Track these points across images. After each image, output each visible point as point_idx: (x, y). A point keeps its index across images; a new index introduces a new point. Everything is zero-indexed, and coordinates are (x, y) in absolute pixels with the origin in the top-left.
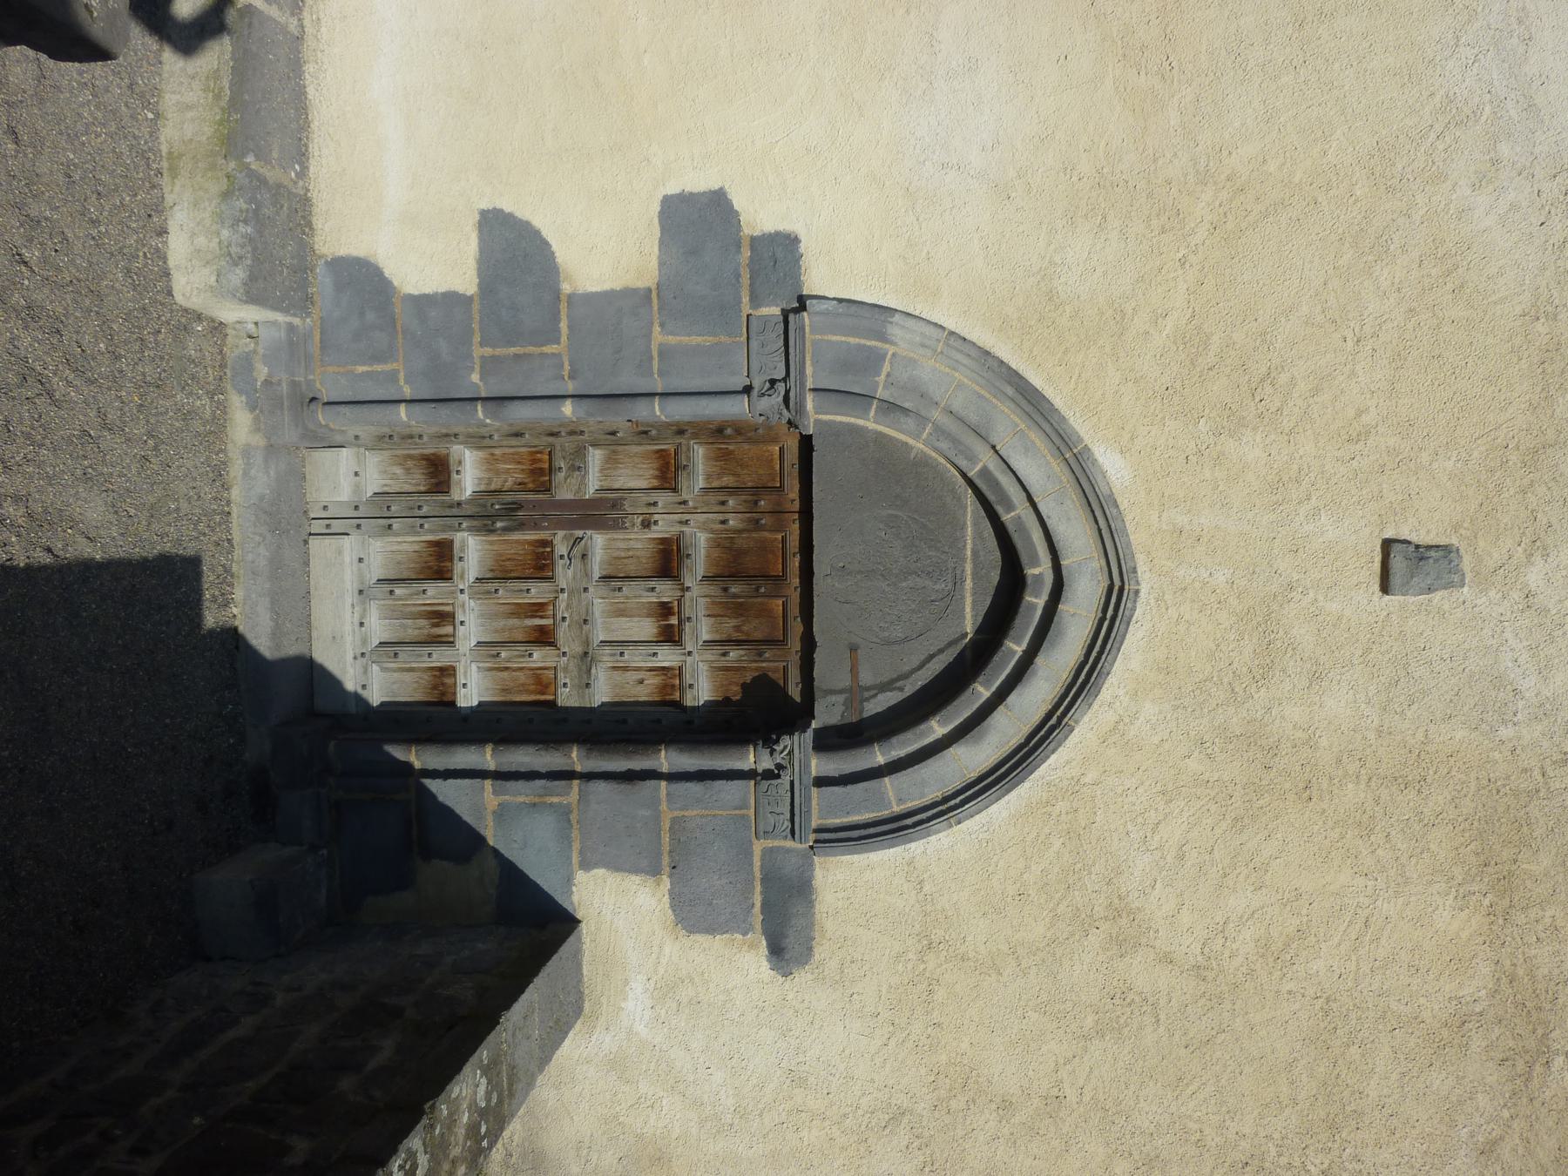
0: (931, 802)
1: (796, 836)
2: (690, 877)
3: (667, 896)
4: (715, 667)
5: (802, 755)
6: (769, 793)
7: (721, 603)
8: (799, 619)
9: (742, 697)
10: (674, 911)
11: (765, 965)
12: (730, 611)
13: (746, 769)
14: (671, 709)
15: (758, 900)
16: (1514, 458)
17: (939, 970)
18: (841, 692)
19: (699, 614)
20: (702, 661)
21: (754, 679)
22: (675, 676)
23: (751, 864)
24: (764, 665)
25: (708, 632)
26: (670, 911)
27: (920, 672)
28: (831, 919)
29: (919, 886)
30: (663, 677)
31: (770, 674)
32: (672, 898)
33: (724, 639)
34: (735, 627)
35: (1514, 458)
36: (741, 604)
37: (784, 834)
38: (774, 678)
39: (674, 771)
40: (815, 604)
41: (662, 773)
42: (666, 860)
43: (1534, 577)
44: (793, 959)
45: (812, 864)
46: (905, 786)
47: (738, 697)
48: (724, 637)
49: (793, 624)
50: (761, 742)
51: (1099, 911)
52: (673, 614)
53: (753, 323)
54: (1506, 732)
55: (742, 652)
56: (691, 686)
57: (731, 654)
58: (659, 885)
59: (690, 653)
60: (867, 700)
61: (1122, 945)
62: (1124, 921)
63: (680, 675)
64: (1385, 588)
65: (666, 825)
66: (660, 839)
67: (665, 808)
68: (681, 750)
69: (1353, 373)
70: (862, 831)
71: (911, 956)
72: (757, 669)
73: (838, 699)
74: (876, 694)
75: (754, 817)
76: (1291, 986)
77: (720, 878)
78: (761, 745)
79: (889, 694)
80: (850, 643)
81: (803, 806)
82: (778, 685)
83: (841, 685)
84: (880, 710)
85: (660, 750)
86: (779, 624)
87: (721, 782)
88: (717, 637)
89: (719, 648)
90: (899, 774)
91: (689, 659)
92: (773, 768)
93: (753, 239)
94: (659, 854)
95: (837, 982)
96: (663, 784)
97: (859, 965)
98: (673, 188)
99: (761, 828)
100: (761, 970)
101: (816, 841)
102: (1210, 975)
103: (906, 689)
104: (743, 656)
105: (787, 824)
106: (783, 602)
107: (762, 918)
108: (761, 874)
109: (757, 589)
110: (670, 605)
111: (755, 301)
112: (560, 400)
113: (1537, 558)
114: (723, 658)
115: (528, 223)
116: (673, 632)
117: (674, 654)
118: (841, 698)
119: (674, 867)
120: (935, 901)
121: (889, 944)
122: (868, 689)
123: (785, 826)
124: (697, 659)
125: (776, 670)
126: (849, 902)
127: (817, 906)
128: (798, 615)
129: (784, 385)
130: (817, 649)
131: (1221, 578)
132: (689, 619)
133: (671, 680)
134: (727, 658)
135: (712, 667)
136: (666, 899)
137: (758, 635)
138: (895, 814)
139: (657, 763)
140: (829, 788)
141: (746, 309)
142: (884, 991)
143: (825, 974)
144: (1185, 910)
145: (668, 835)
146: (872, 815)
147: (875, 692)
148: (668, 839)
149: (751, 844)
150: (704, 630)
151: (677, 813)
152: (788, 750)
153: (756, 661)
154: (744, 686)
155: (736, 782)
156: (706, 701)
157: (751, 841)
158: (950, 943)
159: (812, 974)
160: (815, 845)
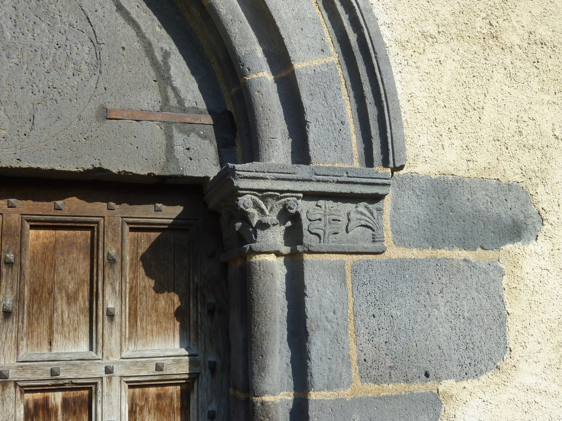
0: (324, 12)
1: (377, 194)
2: (438, 351)
3: (464, 383)
4: (130, 333)
5: (267, 175)
6: (321, 232)
7: (30, 324)
8: (59, 203)
9: (177, 292)
10: (482, 372)
11: (532, 246)
12: (44, 309)
13: (285, 271)
14: (193, 397)
15: (459, 254)
17: (518, 31)
18: (169, 137)
19: (46, 357)
20: (121, 350)
21: (149, 274)
22: (143, 394)
23: (416, 261)
24: (128, 258)
25: (76, 342)
26: (483, 378)
27: (143, 28)
28: (474, 157)
29: (430, 40)
30: (145, 412)
31: (141, 251)
32: (467, 376)
33: (88, 319)
34: (69, 304)
36: (34, 292)
37: (375, 212)
38: (147, 246)
39: (291, 382)
40: (34, 165)
41: (295, 400)
44: (523, 209)
46: (304, 42)
47: (176, 298)
48: (84, 320)
49: (66, 212)
50: (247, 247)
52: (46, 400)
55: (108, 289)
56: (159, 368)
57: (110, 306)
58: (451, 397)
59: (109, 371)
60: (181, 101)
63: (142, 385)
65: (372, 389)
66: (391, 397)
67: (349, 391)
68: (263, 369)
70: (367, 101)
71: (508, 62)
72: (134, 272)
73: (180, 141)
74: (174, 89)
75: (354, 257)
77: (437, 307)
78: (253, 245)
79: (173, 72)
80: (97, 118)
81: (340, 179)
82: (158, 240)
83: (160, 137)
84: (195, 86)
85: (262, 403)
86: (66, 237)
87: (308, 305)
88: (85, 329)
89: (100, 325)
90: (289, 48)
91: (118, 372)
92: (283, 228)
94: (411, 397)
95: (544, 155)
96: (313, 396)
97: (523, 125)
99: (369, 246)
100: (540, 253)
101: (385, 163)
103: (166, 47)
104: (113, 289)
105: (362, 206)
106: (32, 227)
107: (479, 249)
108: (428, 248)
109: (9, 264)
110: (31, 405)
114: (117, 319)
116: (75, 400)
117: (109, 395)
118: (179, 139)
119: (427, 375)
120: (445, 22)
121: (498, 85)
122: (166, 100)
123: (365, 212)
124: (117, 359)
125: (136, 243)
126: (454, 131)
127: (460, 174)
128: (52, 203)
130: (105, 167)
132: (53, 373)
133: (150, 399)
134: (117, 312)
135: (130, 338)
136: (469, 384)
137: (83, 267)
138: (342, 58)
139: (280, 410)
140: (311, 147)
142: (547, 98)
143: (536, 169)
145: (385, 385)
146: (344, 92)
147: (169, 90)
148: (391, 386)
149: (389, 261)
150: (74, 351)
151: (355, 374)
152: (261, 202)
153: (122, 269)
154: (159, 289)
155: (307, 282)
156: (181, 346)
157: (386, 262)
158: (489, 12)
159: (537, 185)
160: (391, 165)
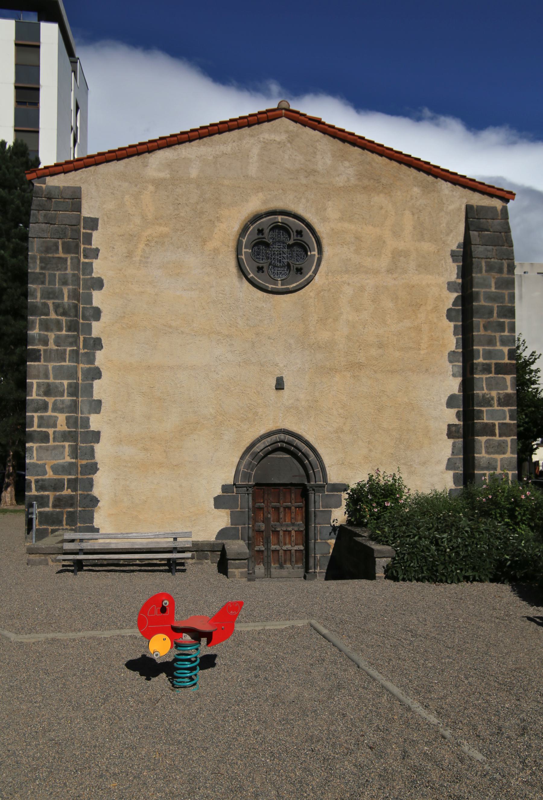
16: (262, 368)
35: (262, 368)
42: (329, 509)
43: (281, 365)
45: (330, 484)
51: (337, 435)
53: (238, 493)
54: (307, 370)
61: (342, 431)
62: (338, 431)
64: (283, 389)
69: (248, 394)
76: (349, 404)
93: (222, 493)
98: (213, 507)
102: (347, 417)
111: (233, 492)
112: (240, 260)
113: (278, 365)
115: (218, 533)
129: (247, 487)
131: (281, 415)
141: (234, 494)
144: (336, 421)
